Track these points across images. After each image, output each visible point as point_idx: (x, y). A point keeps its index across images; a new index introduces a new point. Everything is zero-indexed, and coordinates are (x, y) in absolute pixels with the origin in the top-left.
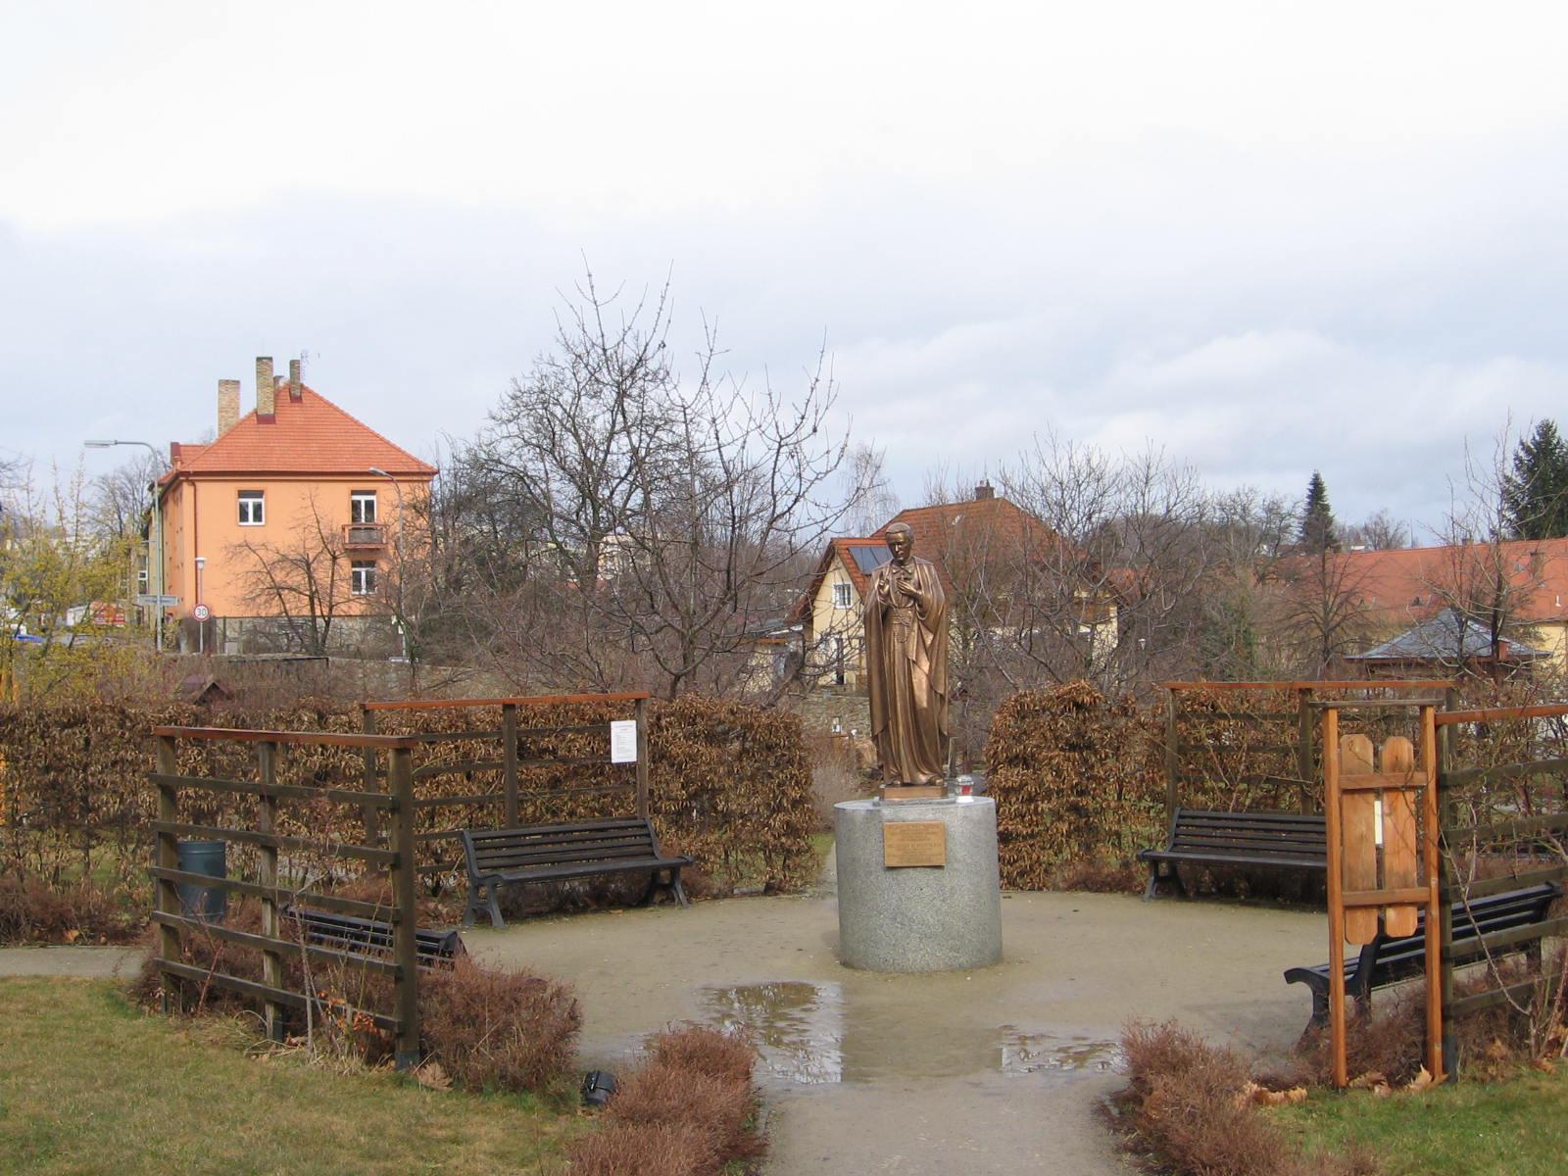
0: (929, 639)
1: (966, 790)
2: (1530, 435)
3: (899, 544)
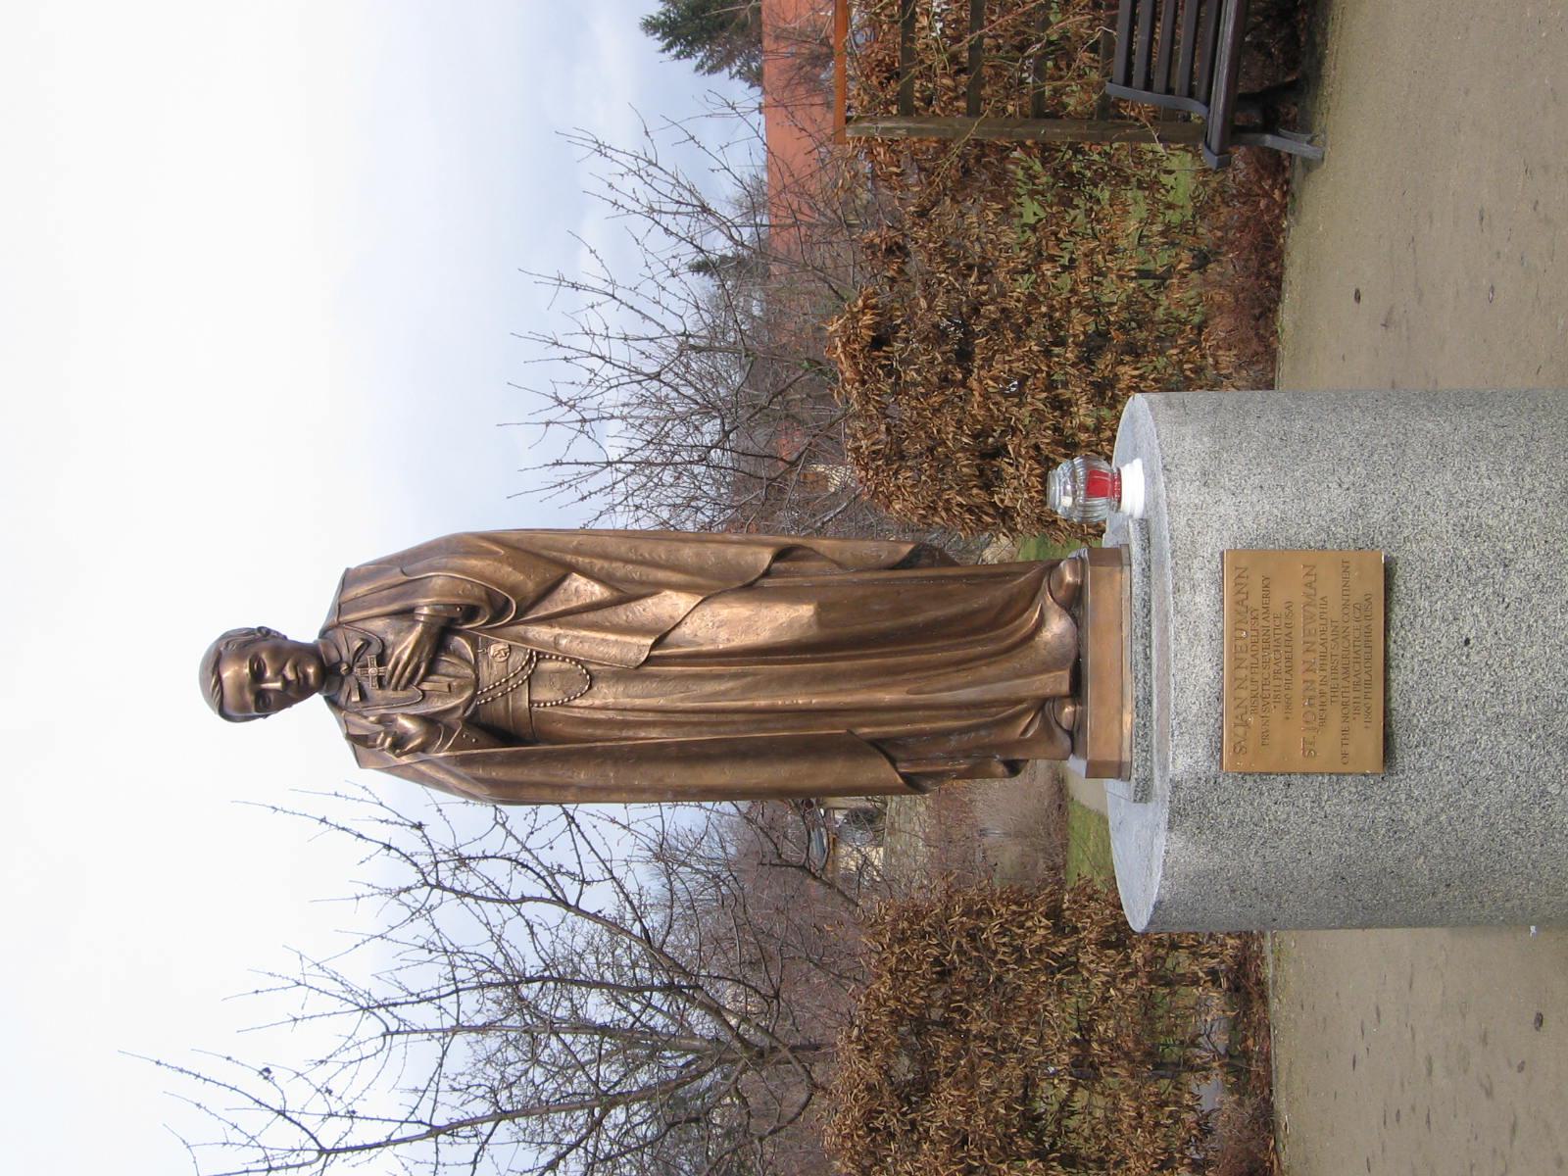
0: (583, 589)
1: (1102, 486)
2: (655, 43)
3: (257, 675)
